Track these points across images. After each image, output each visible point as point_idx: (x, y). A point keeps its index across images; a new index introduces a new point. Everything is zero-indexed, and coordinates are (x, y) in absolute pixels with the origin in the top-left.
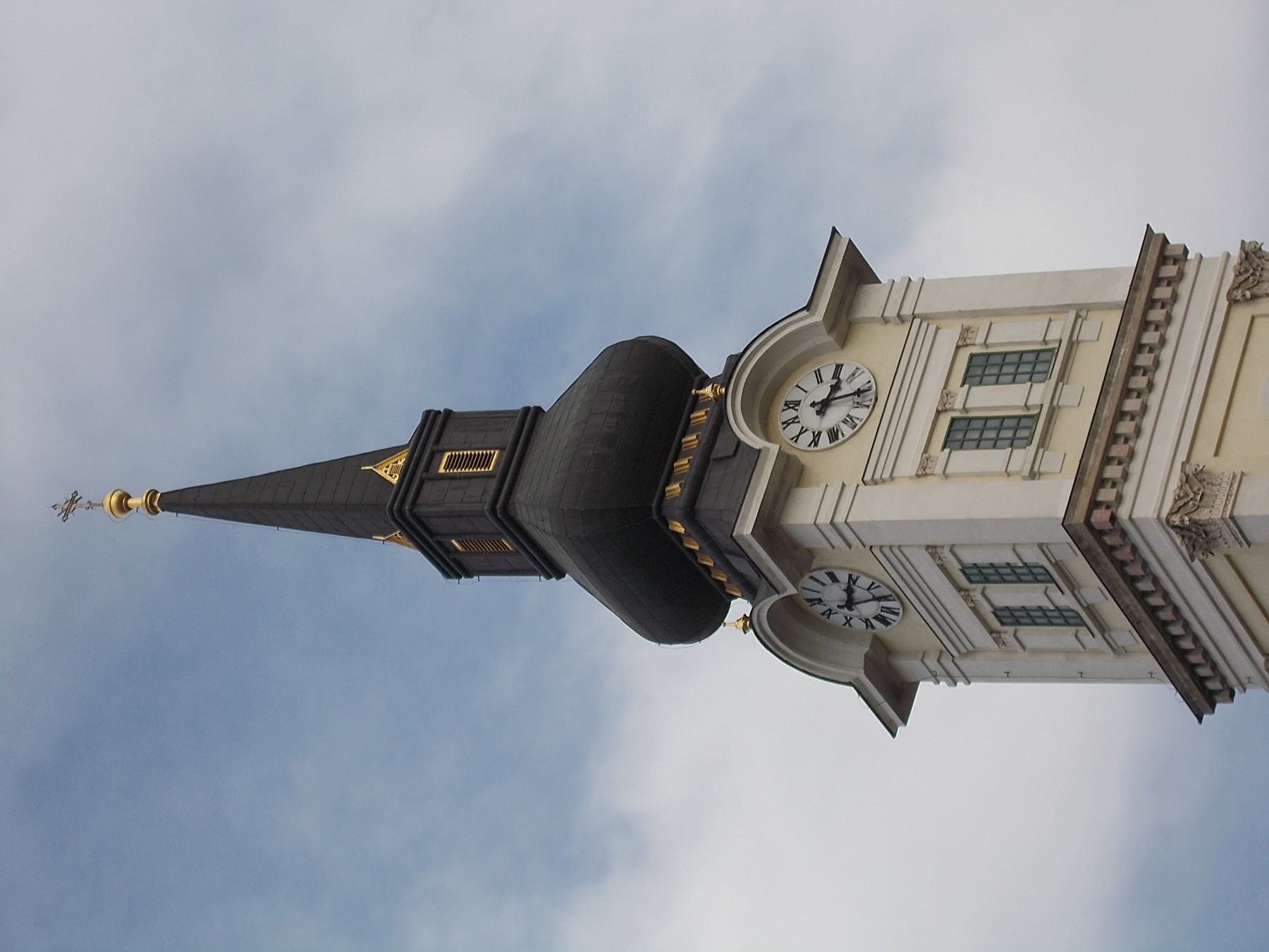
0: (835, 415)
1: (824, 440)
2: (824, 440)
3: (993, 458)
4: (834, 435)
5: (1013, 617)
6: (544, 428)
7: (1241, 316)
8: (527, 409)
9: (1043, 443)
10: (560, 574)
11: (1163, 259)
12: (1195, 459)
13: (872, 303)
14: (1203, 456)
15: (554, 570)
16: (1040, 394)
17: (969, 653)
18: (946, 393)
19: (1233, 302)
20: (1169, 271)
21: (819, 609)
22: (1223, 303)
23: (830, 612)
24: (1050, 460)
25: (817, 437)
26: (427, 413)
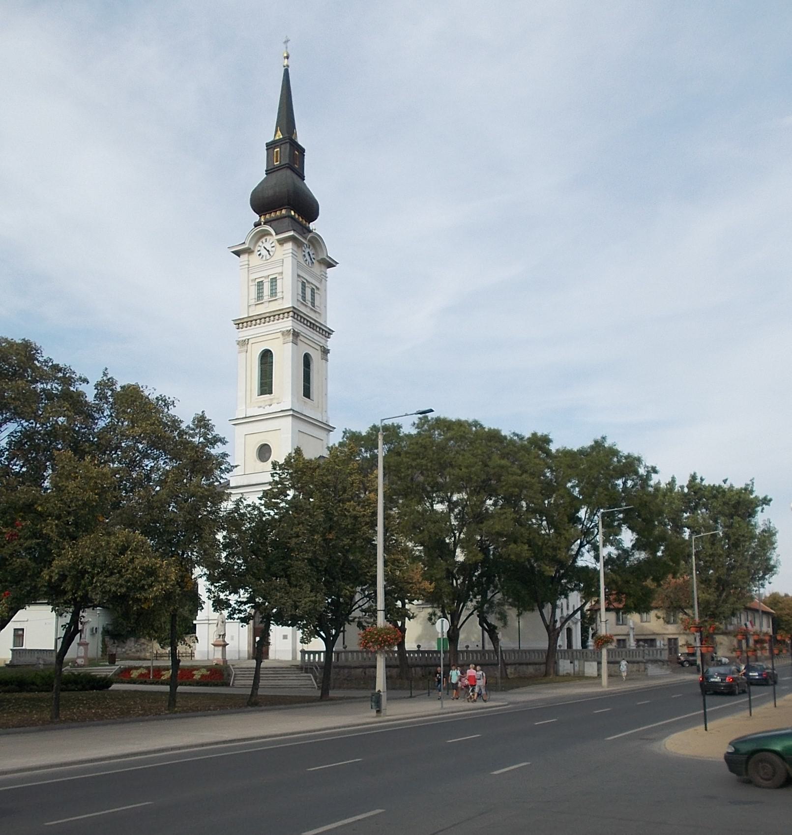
0: (307, 255)
1: (304, 253)
2: (304, 253)
3: (300, 293)
4: (304, 256)
5: (260, 285)
6: (299, 179)
7: (318, 348)
8: (304, 177)
10: (266, 174)
11: (329, 334)
12: (301, 337)
13: (323, 267)
14: (301, 338)
15: (268, 172)
16: (309, 305)
17: (248, 271)
19: (321, 347)
20: (327, 335)
21: (264, 241)
22: (321, 345)
23: (262, 242)
24: (299, 304)
25: (304, 251)
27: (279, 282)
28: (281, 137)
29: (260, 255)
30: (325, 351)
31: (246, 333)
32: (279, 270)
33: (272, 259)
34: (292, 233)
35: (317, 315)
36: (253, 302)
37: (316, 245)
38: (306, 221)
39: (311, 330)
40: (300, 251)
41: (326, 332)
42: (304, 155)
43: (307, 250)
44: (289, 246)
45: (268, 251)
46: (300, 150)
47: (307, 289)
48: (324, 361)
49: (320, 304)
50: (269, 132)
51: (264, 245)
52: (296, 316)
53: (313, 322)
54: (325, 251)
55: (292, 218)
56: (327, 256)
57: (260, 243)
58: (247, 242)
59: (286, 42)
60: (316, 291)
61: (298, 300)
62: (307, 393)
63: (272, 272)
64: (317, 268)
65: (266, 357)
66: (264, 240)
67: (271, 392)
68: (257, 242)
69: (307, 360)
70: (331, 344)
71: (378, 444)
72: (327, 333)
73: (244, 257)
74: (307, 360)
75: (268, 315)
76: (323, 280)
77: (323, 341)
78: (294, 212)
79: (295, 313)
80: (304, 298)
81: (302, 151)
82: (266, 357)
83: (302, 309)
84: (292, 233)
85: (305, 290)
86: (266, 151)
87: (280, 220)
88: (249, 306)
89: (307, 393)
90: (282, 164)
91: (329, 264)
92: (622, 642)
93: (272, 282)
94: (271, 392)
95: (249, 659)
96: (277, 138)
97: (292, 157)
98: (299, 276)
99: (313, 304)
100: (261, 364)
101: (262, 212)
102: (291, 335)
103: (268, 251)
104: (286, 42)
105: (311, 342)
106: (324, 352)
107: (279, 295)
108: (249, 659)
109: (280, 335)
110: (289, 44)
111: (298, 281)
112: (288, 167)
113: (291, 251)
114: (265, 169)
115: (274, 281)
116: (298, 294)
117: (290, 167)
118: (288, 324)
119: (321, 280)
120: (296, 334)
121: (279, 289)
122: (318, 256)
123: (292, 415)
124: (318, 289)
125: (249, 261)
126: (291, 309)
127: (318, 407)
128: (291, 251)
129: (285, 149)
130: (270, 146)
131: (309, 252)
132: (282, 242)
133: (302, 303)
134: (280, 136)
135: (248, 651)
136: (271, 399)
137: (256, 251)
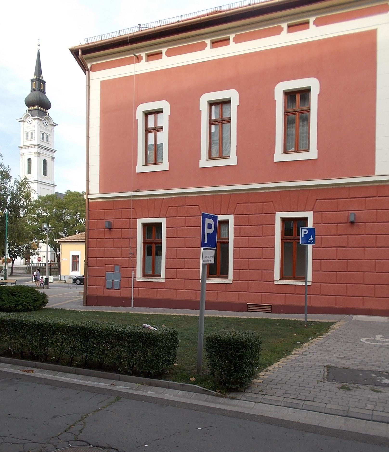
4: (44, 124)
5: (27, 134)
6: (44, 94)
7: (50, 157)
9: (42, 141)
11: (54, 151)
13: (52, 127)
14: (41, 154)
18: (45, 133)
20: (53, 152)
24: (41, 142)
26: (45, 82)
27: (33, 134)
28: (36, 78)
29: (27, 123)
30: (53, 158)
31: (22, 151)
32: (33, 129)
33: (31, 125)
34: (37, 117)
35: (50, 145)
36: (25, 140)
37: (49, 119)
38: (45, 110)
39: (46, 151)
40: (42, 123)
41: (53, 151)
42: (45, 84)
43: (45, 121)
44: (37, 121)
45: (30, 122)
46: (43, 82)
47: (44, 136)
48: (52, 162)
49: (51, 140)
50: (32, 75)
51: (29, 119)
52: (39, 147)
53: (47, 148)
54: (52, 121)
55: (39, 110)
56: (53, 122)
57: (27, 119)
58: (23, 118)
59: (39, 39)
60: (49, 136)
61: (40, 141)
62: (45, 173)
63: (31, 129)
64: (49, 127)
65: (29, 160)
66: (28, 117)
67: (31, 174)
68: (26, 118)
69: (45, 162)
70: (55, 155)
71: (18, 359)
72: (54, 151)
73: (22, 123)
74: (45, 162)
75: (29, 146)
76: (52, 132)
77: (52, 154)
78: (40, 107)
79: (38, 146)
80: (43, 139)
81: (44, 83)
82: (29, 160)
83: (43, 144)
84: (37, 117)
85: (44, 136)
86: (31, 83)
87: (35, 110)
88: (24, 141)
89: (45, 173)
90: (36, 88)
91: (55, 125)
92: (154, 229)
93: (31, 133)
94: (31, 174)
95: (24, 265)
96: (35, 78)
97: (40, 85)
98: (41, 131)
99: (47, 141)
100: (28, 163)
101: (32, 106)
102: (37, 154)
103: (30, 122)
104: (39, 39)
105: (46, 156)
106: (52, 158)
107: (33, 139)
108: (24, 265)
109: (33, 153)
110: (40, 40)
111: (40, 133)
112: (38, 90)
113: (37, 123)
114: (30, 89)
115: (32, 133)
116: (40, 138)
117: (39, 90)
118: (36, 149)
119: (51, 132)
120: (39, 154)
121: (33, 137)
122: (49, 123)
123: (37, 183)
124: (50, 135)
125: (24, 125)
126: (37, 145)
127: (50, 178)
128: (37, 123)
129: (37, 83)
130: (32, 81)
131: (45, 122)
132: (34, 119)
133: (42, 141)
134: (35, 78)
135: (24, 262)
136: (31, 176)
137: (26, 121)
